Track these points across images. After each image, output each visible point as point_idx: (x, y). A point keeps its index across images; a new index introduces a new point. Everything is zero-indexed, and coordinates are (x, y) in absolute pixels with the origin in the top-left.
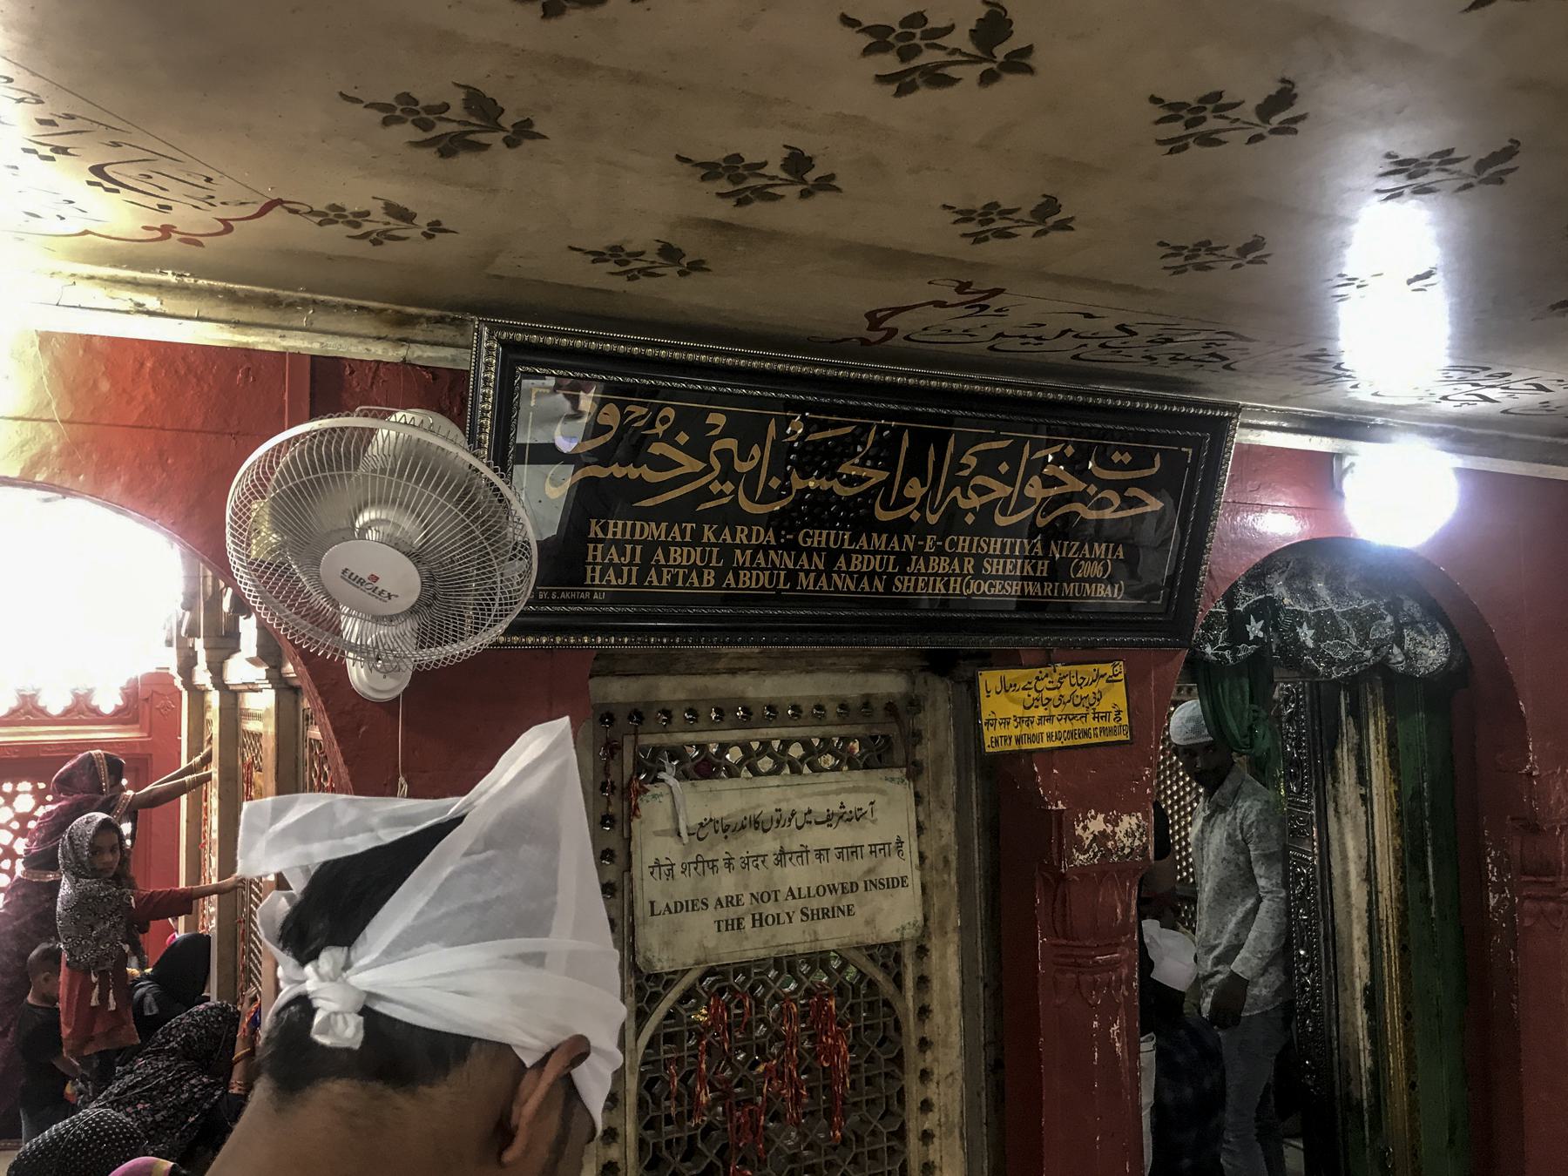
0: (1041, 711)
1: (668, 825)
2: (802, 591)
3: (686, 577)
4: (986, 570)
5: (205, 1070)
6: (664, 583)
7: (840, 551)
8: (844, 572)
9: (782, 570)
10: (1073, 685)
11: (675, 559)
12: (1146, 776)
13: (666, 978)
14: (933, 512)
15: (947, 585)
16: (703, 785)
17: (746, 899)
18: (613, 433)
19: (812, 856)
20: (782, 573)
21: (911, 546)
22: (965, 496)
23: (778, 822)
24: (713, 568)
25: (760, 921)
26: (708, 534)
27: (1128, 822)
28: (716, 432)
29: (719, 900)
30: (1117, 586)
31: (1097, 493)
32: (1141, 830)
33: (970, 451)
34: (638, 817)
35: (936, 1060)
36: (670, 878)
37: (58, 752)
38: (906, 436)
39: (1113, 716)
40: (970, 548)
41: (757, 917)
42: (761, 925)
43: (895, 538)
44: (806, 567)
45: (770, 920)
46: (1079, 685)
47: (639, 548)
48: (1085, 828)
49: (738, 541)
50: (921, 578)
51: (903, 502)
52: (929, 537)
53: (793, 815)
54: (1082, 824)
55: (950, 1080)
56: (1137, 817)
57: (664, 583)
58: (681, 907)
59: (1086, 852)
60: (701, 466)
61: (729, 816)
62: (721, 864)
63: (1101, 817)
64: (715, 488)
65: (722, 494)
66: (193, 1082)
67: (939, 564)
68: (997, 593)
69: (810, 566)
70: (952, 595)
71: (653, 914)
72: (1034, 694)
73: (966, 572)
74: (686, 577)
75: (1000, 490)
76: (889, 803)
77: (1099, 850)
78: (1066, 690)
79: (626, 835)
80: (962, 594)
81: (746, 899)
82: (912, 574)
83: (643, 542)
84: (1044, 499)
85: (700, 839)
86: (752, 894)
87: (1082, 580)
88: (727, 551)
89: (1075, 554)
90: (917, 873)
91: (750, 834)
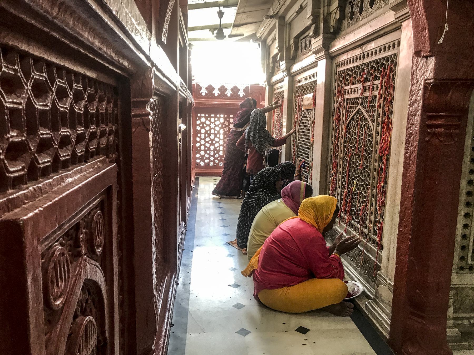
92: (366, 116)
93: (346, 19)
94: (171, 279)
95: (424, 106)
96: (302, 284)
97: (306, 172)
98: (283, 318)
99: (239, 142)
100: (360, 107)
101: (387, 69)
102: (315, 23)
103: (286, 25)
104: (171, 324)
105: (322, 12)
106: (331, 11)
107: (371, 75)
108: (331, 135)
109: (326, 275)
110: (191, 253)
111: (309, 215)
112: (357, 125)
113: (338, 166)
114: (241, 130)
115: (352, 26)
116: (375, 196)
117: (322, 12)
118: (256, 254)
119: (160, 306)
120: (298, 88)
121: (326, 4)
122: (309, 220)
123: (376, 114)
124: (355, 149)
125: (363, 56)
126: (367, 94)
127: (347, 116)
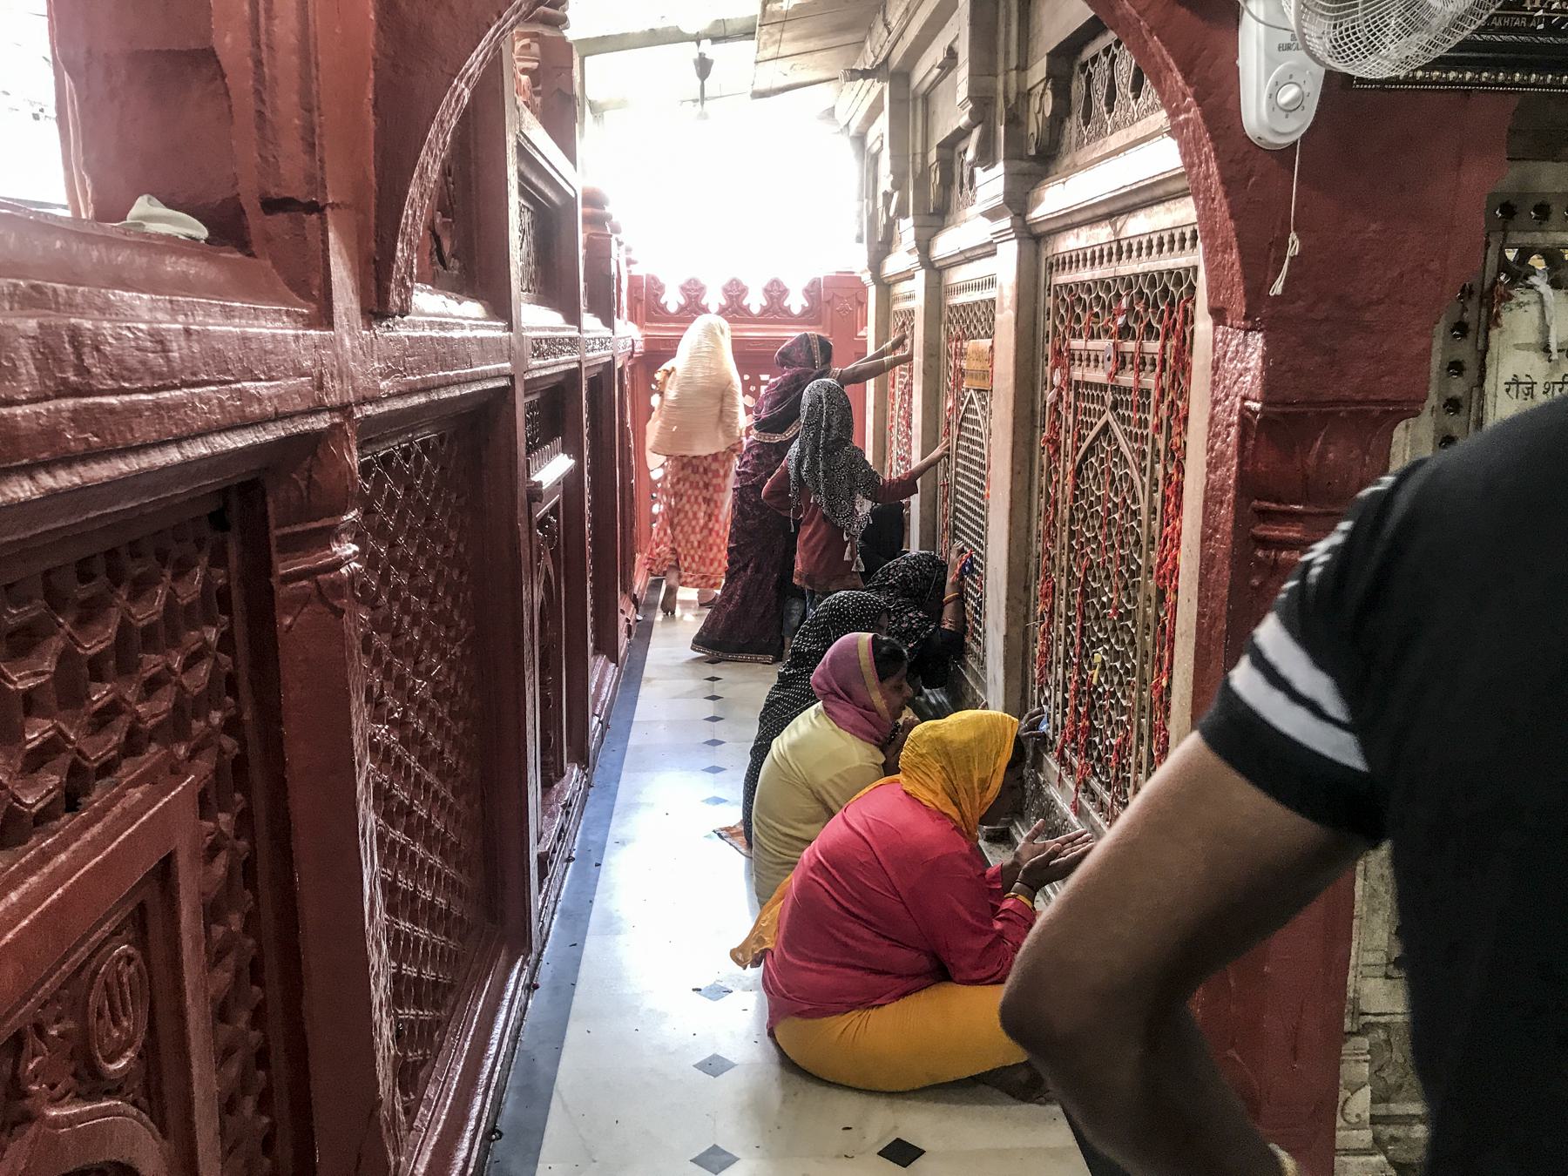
1: (1533, 337)
5: (920, 607)
34: (1498, 326)
36: (1529, 397)
37: (760, 347)
66: (911, 615)
79: (1480, 345)
92: (1124, 449)
93: (1074, 117)
94: (506, 978)
95: (1241, 478)
96: (909, 1001)
97: (977, 592)
98: (848, 1106)
99: (772, 486)
100: (1109, 416)
101: (1178, 312)
102: (980, 123)
103: (915, 99)
104: (494, 1131)
105: (1000, 87)
106: (1029, 87)
107: (1138, 318)
108: (1036, 490)
109: (981, 974)
110: (593, 869)
111: (928, 780)
112: (1103, 473)
113: (1056, 594)
114: (778, 438)
115: (1088, 144)
116: (1147, 710)
117: (1000, 87)
118: (776, 895)
119: (455, 1082)
120: (954, 310)
121: (1013, 64)
122: (930, 797)
123: (1148, 449)
124: (1098, 547)
125: (1119, 250)
126: (1127, 379)
127: (1076, 437)
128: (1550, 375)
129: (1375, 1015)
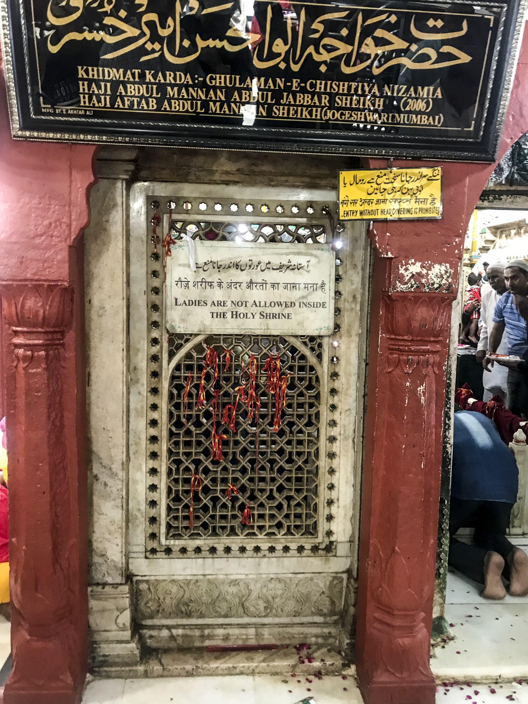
0: (379, 196)
2: (212, 114)
3: (139, 104)
4: (338, 104)
6: (126, 107)
7: (234, 88)
8: (238, 102)
9: (199, 100)
10: (403, 181)
11: (131, 92)
12: (456, 242)
13: (185, 337)
14: (296, 63)
15: (310, 113)
16: (208, 243)
17: (229, 303)
18: (80, 11)
19: (269, 286)
20: (199, 102)
21: (282, 86)
22: (318, 52)
23: (250, 266)
24: (154, 98)
25: (235, 315)
26: (149, 77)
27: (438, 269)
28: (142, 9)
29: (213, 302)
30: (437, 117)
31: (417, 50)
32: (448, 274)
33: (319, 19)
35: (340, 401)
38: (269, 8)
39: (429, 201)
40: (325, 88)
41: (234, 313)
42: (236, 317)
43: (270, 81)
44: (214, 98)
45: (242, 316)
46: (407, 181)
47: (109, 85)
48: (406, 270)
49: (168, 81)
50: (291, 108)
51: (272, 56)
52: (294, 80)
53: (259, 263)
54: (404, 267)
55: (348, 412)
56: (446, 267)
57: (126, 107)
58: (191, 303)
59: (406, 283)
60: (137, 32)
61: (221, 261)
62: (215, 284)
63: (418, 264)
64: (149, 46)
65: (153, 51)
67: (303, 99)
68: (346, 119)
69: (216, 98)
70: (313, 119)
71: (176, 304)
72: (375, 186)
73: (323, 104)
74: (139, 104)
75: (344, 48)
76: (319, 262)
77: (415, 283)
78: (397, 184)
80: (322, 119)
81: (229, 303)
82: (285, 105)
83: (111, 81)
84: (377, 55)
85: (204, 271)
86: (232, 302)
87: (410, 112)
88: (162, 88)
89: (403, 94)
90: (333, 301)
91: (233, 271)
128: (196, 278)
129: (142, 576)
